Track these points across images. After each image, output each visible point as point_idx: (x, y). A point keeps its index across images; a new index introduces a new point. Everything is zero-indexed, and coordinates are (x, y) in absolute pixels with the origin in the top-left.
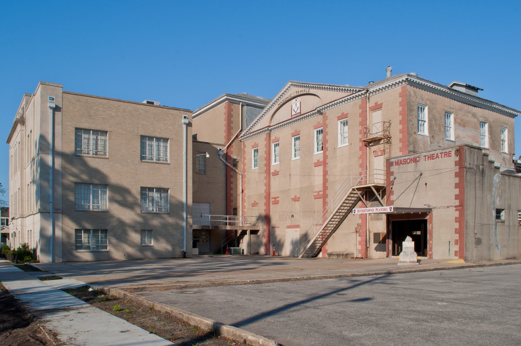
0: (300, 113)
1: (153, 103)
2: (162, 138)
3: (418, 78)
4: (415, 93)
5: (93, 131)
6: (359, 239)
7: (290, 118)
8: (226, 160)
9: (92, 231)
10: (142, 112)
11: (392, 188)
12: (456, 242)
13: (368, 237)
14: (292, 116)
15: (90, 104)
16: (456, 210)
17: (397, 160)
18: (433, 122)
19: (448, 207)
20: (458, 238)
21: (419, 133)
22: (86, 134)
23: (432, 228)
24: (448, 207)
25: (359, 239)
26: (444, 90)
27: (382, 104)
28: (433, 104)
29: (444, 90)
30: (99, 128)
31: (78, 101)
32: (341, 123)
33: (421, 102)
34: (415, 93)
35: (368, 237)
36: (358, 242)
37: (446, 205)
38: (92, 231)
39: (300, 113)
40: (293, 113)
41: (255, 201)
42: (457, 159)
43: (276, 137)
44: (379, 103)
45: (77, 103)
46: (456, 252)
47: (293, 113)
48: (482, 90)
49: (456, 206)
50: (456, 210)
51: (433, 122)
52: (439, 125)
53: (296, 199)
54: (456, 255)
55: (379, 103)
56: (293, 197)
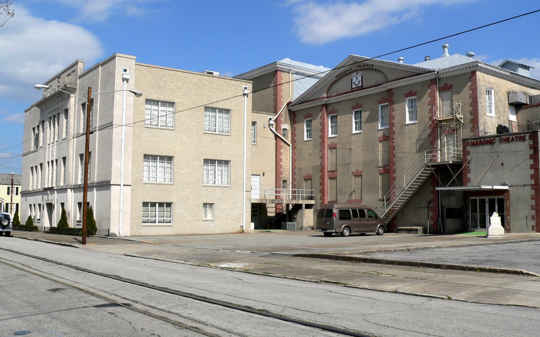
0: (362, 86)
1: (212, 73)
2: (224, 109)
3: (486, 64)
4: (483, 77)
5: (162, 102)
6: (431, 214)
7: (350, 90)
8: (276, 130)
9: (157, 205)
10: (206, 83)
11: (468, 167)
12: (533, 218)
13: (440, 213)
14: (352, 89)
15: (159, 75)
16: (532, 189)
17: (473, 141)
18: (499, 104)
19: (524, 186)
20: (534, 214)
21: (488, 114)
22: (170, 107)
23: (509, 204)
24: (524, 186)
25: (431, 214)
26: (507, 74)
27: (452, 86)
28: (498, 87)
29: (507, 74)
30: (167, 99)
31: (149, 72)
32: (409, 100)
33: (488, 86)
34: (483, 77)
35: (440, 213)
36: (430, 217)
37: (522, 183)
38: (157, 205)
39: (362, 86)
40: (354, 86)
41: (308, 174)
42: (532, 143)
43: (333, 109)
44: (448, 84)
45: (148, 74)
46: (533, 227)
47: (354, 86)
48: (533, 68)
49: (531, 185)
50: (532, 189)
51: (499, 104)
52: (504, 106)
53: (358, 175)
54: (533, 229)
55: (448, 84)
56: (354, 170)
